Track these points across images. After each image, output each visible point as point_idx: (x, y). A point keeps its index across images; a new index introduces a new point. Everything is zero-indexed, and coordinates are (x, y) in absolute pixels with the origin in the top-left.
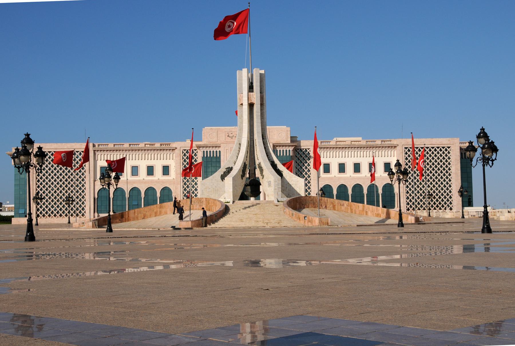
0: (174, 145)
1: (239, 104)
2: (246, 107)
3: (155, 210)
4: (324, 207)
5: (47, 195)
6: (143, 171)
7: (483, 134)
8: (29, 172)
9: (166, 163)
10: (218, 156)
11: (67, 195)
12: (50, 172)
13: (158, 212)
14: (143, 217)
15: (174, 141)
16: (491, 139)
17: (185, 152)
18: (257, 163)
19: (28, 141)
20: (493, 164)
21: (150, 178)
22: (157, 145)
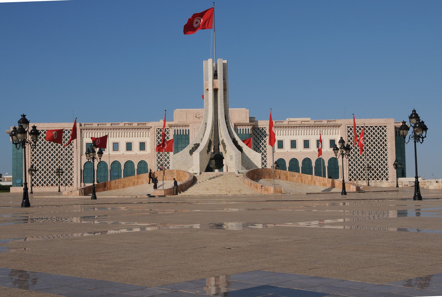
0: (149, 124)
1: (205, 89)
2: (211, 92)
3: (133, 181)
4: (278, 177)
7: (414, 115)
9: (142, 140)
10: (187, 134)
11: (57, 167)
12: (43, 147)
13: (136, 182)
15: (149, 121)
16: (422, 119)
17: (159, 130)
18: (221, 139)
19: (24, 121)
20: (423, 141)
22: (135, 125)
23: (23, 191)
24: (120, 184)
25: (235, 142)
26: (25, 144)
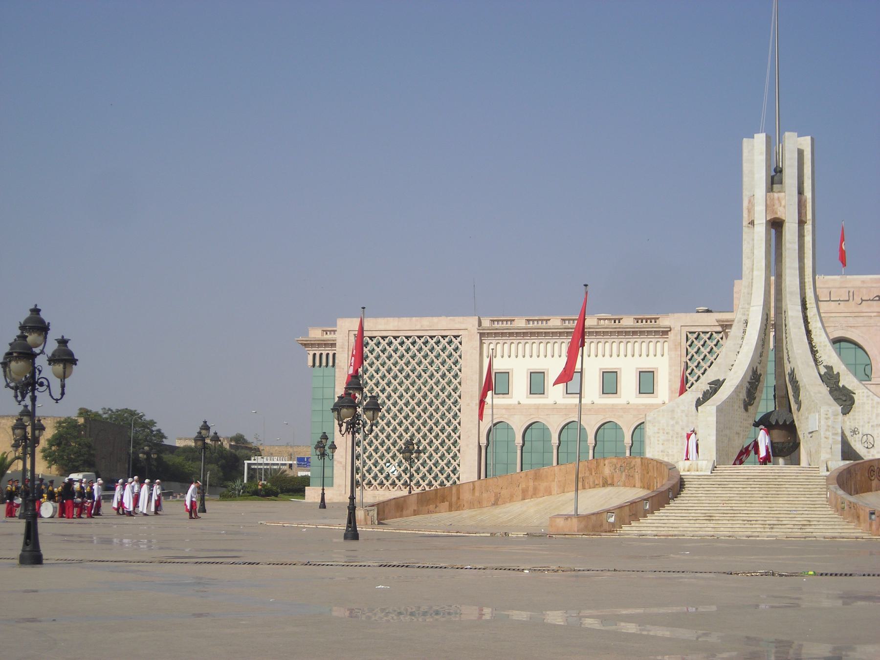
0: (665, 321)
1: (745, 223)
2: (760, 229)
3: (523, 485)
6: (628, 383)
9: (646, 364)
11: (407, 437)
12: (383, 383)
13: (531, 489)
14: (493, 499)
15: (668, 311)
17: (692, 337)
19: (36, 324)
21: (610, 400)
22: (628, 322)
23: (348, 501)
24: (485, 495)
26: (33, 390)
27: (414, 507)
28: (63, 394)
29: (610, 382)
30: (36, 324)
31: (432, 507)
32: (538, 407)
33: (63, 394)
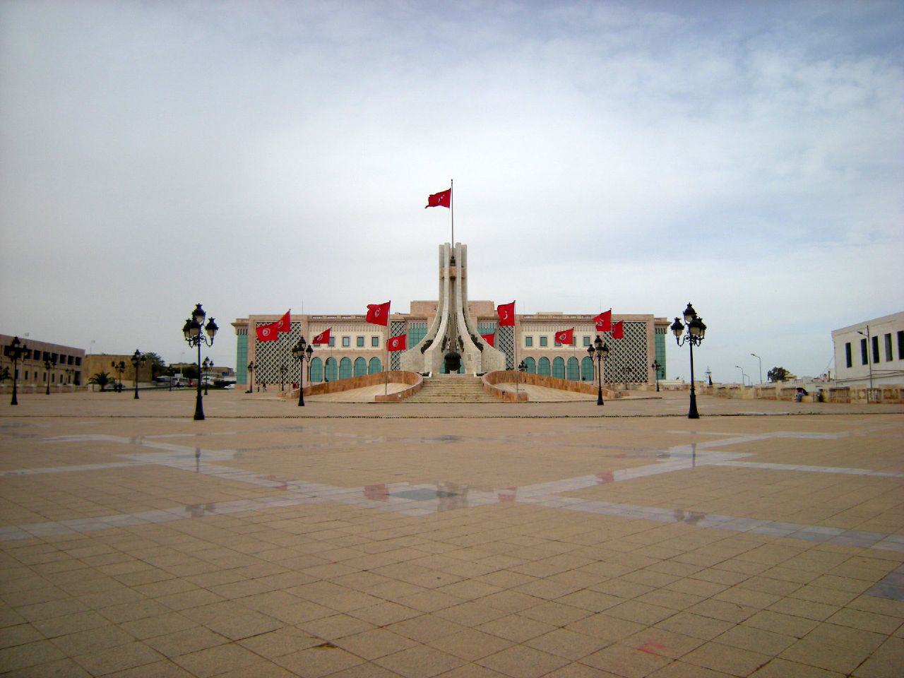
4: (523, 381)
5: (260, 363)
7: (690, 312)
8: (199, 345)
16: (699, 315)
18: (458, 335)
19: (199, 312)
20: (700, 343)
21: (376, 349)
25: (474, 339)
26: (199, 341)
27: (310, 392)
28: (212, 343)
29: (529, 341)
30: (199, 312)
31: (317, 392)
32: (560, 352)
33: (212, 343)
